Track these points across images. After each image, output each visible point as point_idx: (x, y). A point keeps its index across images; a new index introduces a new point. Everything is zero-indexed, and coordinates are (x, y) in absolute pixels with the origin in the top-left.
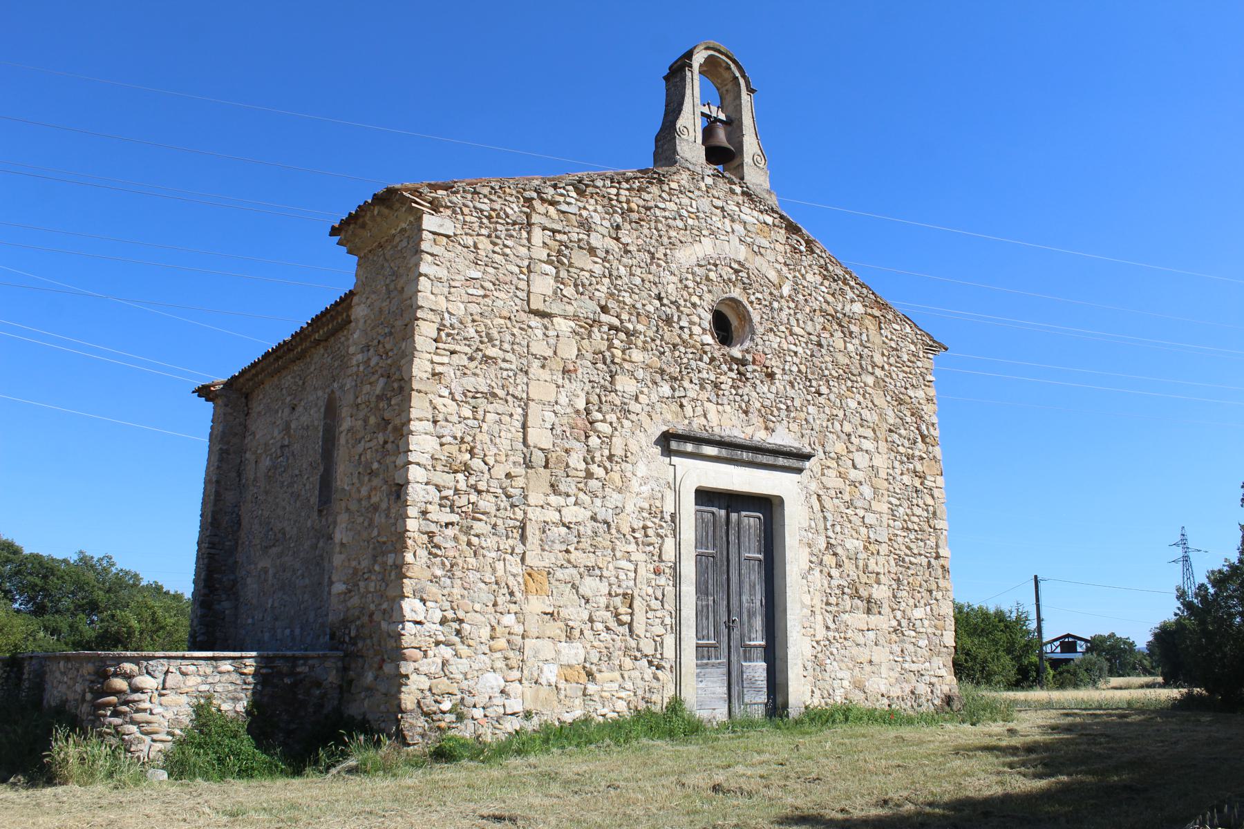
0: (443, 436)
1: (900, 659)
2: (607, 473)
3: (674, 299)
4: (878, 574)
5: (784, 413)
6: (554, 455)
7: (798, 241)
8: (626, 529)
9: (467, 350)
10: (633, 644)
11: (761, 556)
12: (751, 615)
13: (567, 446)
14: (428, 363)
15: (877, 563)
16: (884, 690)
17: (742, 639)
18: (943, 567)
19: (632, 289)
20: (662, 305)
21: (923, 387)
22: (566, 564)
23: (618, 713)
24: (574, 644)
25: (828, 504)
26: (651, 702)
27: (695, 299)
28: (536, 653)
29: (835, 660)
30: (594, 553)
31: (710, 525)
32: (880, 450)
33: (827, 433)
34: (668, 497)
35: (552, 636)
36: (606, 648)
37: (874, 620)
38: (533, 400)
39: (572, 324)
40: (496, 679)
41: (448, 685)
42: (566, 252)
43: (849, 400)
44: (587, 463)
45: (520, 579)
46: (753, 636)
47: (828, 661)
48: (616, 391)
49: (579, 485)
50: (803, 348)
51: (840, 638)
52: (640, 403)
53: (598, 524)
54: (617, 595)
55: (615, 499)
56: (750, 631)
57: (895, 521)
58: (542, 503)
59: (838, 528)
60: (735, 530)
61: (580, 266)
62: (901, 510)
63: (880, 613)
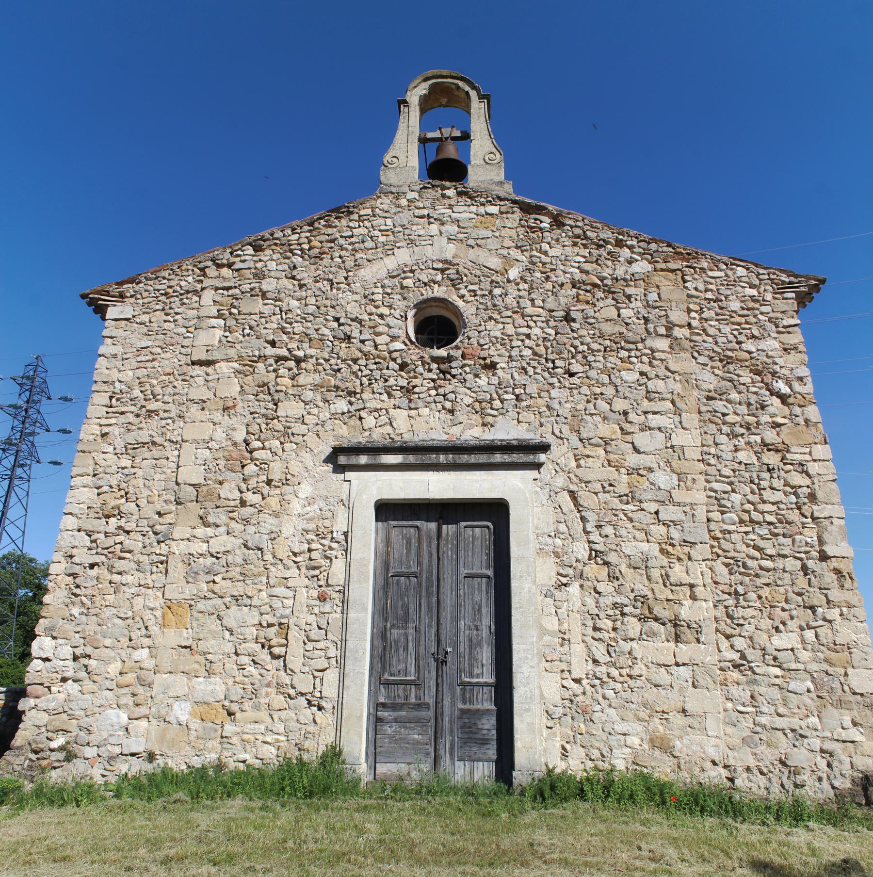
0: (101, 487)
1: (750, 709)
2: (263, 499)
3: (354, 317)
4: (692, 586)
5: (509, 405)
6: (205, 489)
7: (536, 219)
8: (283, 553)
9: (133, 409)
11: (490, 573)
12: (474, 644)
13: (220, 478)
14: (98, 427)
15: (687, 572)
16: (712, 753)
17: (459, 671)
18: (837, 572)
19: (305, 318)
20: (340, 325)
21: (776, 335)
23: (262, 759)
24: (212, 680)
25: (585, 498)
27: (385, 311)
28: (166, 688)
29: (610, 706)
30: (244, 581)
31: (414, 541)
32: (685, 425)
33: (584, 417)
34: (340, 515)
36: (252, 684)
37: (685, 651)
38: (187, 441)
39: (235, 365)
40: (118, 716)
41: (64, 722)
42: (236, 303)
43: (623, 373)
44: (241, 492)
45: (158, 613)
46: (476, 671)
47: (597, 708)
48: (278, 417)
49: (231, 515)
50: (542, 328)
51: (621, 675)
52: (306, 424)
53: (251, 551)
54: (270, 625)
55: (269, 523)
56: (471, 666)
57: (723, 513)
58: (188, 536)
59: (609, 530)
60: (452, 544)
61: (248, 312)
62: (736, 498)
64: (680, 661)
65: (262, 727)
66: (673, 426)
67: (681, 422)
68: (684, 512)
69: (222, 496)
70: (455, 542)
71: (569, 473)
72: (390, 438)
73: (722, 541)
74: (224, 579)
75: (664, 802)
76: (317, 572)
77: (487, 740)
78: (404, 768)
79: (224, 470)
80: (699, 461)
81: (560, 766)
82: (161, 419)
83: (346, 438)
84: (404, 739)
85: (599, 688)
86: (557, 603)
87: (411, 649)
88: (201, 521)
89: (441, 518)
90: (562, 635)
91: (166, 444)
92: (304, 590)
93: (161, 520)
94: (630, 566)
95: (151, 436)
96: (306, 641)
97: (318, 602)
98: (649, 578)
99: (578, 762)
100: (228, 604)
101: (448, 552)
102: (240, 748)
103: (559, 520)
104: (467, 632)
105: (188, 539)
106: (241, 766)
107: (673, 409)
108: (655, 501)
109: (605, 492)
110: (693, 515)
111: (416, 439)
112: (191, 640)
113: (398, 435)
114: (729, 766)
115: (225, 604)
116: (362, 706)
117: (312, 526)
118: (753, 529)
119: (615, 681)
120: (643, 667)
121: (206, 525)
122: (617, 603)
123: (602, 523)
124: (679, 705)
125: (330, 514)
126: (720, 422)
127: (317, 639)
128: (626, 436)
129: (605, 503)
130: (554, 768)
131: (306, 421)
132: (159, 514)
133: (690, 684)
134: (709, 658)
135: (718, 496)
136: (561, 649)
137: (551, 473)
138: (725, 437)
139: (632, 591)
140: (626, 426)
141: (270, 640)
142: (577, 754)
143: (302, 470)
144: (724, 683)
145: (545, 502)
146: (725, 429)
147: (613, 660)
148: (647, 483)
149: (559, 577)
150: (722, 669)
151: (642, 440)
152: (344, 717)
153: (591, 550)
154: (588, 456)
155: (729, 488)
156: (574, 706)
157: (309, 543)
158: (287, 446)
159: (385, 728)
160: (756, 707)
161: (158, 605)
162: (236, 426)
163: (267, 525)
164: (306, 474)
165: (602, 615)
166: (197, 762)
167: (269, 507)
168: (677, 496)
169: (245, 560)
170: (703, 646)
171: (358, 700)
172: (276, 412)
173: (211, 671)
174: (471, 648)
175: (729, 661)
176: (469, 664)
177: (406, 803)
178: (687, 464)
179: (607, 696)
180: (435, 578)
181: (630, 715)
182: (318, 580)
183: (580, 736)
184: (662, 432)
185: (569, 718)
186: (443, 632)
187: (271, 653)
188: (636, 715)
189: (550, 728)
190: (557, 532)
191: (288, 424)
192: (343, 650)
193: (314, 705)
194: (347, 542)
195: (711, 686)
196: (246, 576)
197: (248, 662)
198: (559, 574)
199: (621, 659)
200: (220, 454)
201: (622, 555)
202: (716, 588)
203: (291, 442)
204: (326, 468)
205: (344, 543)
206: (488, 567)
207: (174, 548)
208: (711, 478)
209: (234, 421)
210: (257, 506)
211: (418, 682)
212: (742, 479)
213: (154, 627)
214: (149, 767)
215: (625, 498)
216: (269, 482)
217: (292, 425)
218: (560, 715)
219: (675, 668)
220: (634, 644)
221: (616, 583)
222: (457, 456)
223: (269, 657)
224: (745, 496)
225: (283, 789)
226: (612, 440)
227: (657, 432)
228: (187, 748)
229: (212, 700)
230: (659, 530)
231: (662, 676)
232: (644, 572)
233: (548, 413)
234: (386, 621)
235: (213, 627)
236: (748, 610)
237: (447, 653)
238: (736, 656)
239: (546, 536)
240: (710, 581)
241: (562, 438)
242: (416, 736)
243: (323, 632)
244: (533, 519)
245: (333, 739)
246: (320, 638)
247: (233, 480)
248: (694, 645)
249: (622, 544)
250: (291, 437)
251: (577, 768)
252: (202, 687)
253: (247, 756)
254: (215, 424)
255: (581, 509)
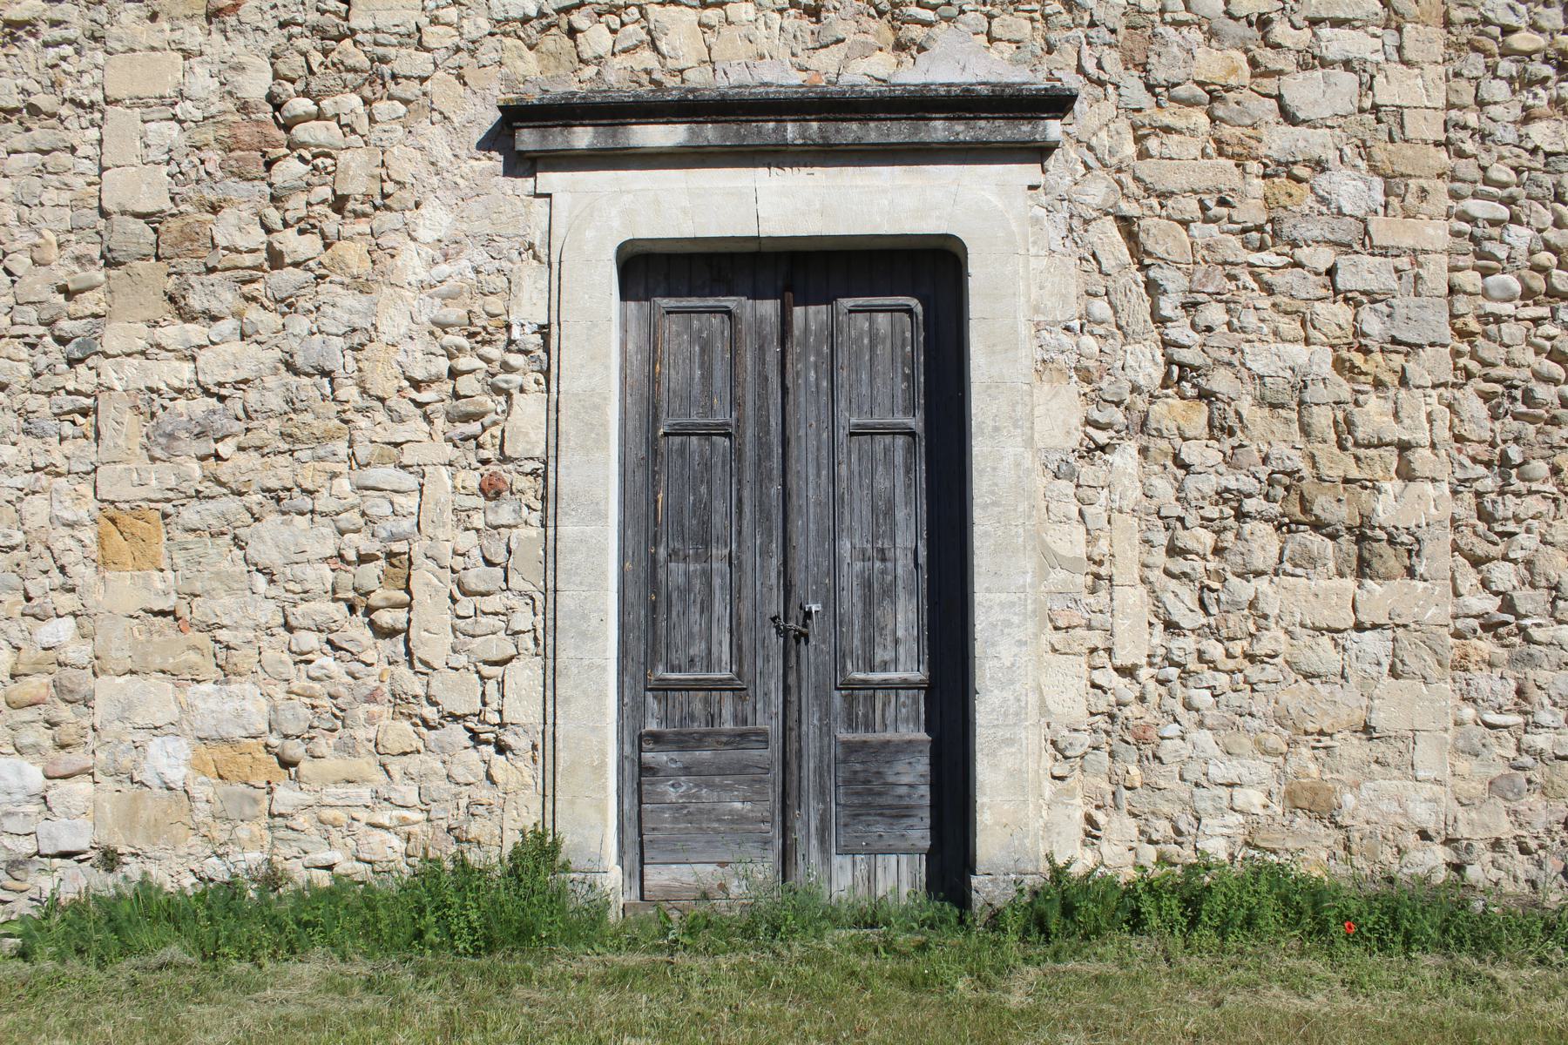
1: (1514, 719)
2: (327, 246)
4: (1404, 447)
6: (174, 224)
8: (385, 381)
10: (416, 686)
11: (916, 422)
12: (875, 593)
13: (213, 197)
15: (1396, 415)
16: (1424, 815)
17: (840, 656)
22: (210, 488)
23: (370, 862)
24: (233, 687)
25: (1160, 236)
26: (469, 841)
28: (125, 711)
29: (1201, 724)
30: (292, 452)
32: (1409, 54)
33: (1160, 29)
34: (527, 283)
35: (167, 667)
36: (332, 697)
37: (1379, 597)
38: (117, 102)
40: (19, 772)
44: (269, 231)
45: (88, 535)
46: (881, 655)
47: (1172, 730)
48: (353, 32)
49: (246, 289)
51: (1229, 655)
52: (428, 50)
53: (305, 380)
54: (363, 559)
55: (345, 306)
56: (869, 643)
57: (1486, 273)
58: (141, 345)
59: (1214, 314)
60: (818, 353)
62: (1520, 236)
63: (1411, 572)
64: (1366, 619)
65: (365, 794)
66: (1380, 57)
67: (1400, 49)
68: (1397, 270)
69: (221, 241)
70: (826, 349)
71: (1119, 170)
72: (652, 81)
73: (1480, 340)
74: (241, 449)
75: (1322, 929)
76: (474, 427)
77: (912, 807)
78: (707, 873)
79: (219, 174)
80: (1437, 144)
81: (1082, 861)
82: (46, 45)
83: (534, 83)
84: (710, 812)
85: (1176, 685)
86: (1083, 492)
87: (720, 608)
88: (171, 307)
89: (788, 288)
90: (1094, 568)
91: (65, 111)
92: (444, 472)
93: (71, 307)
94: (1261, 401)
95: (23, 91)
96: (457, 595)
97: (480, 502)
98: (1305, 430)
99: (1123, 848)
100: (256, 509)
101: (808, 374)
102: (317, 838)
103: (1093, 289)
104: (858, 566)
105: (143, 353)
106: (323, 879)
107: (1383, 13)
108: (1328, 242)
109: (1207, 220)
110: (1417, 277)
111: (722, 83)
112: (174, 597)
113: (672, 73)
114: (1457, 840)
115: (249, 510)
116: (603, 742)
117: (455, 313)
118: (1554, 311)
119: (1216, 669)
120: (1283, 637)
121: (187, 316)
122: (1227, 490)
123: (1200, 297)
124: (1358, 717)
125: (501, 282)
126: (1496, 50)
127: (482, 588)
128: (1265, 81)
129: (1208, 247)
130: (1068, 865)
131: (428, 40)
132: (68, 293)
133: (1386, 668)
134: (1432, 611)
135: (1478, 232)
136: (1091, 600)
137: (1073, 172)
138: (1504, 85)
139: (1265, 460)
140: (1266, 56)
141: (367, 594)
142: (1119, 830)
143: (423, 170)
144: (1461, 665)
145: (1056, 244)
146: (1507, 67)
147: (1212, 621)
148: (1310, 200)
149: (1090, 430)
150: (1458, 635)
151: (1303, 90)
152: (559, 769)
153: (1170, 362)
154: (1168, 130)
155: (1503, 212)
156: (1117, 728)
157: (450, 357)
158: (382, 108)
159: (661, 788)
160: (1526, 713)
161: (83, 514)
162: (243, 59)
163: (338, 313)
164: (435, 180)
165: (1192, 519)
166: (217, 869)
167: (343, 266)
168: (1382, 231)
169: (290, 402)
170: (1420, 585)
171: (594, 729)
172: (346, 19)
173: (229, 668)
174: (868, 601)
175: (1475, 617)
176: (863, 640)
177: (721, 959)
178: (1410, 153)
179: (1196, 703)
180: (775, 439)
181: (1247, 743)
182: (479, 446)
183: (1127, 794)
184: (1353, 70)
185: (1103, 755)
186: (797, 565)
187: (372, 624)
188: (1258, 742)
189: (1061, 778)
190: (1088, 319)
191: (380, 51)
192: (550, 615)
193: (487, 742)
194: (546, 348)
195: (1434, 671)
196: (296, 440)
197: (317, 646)
198: (1089, 422)
199: (1233, 619)
200: (208, 134)
201: (1244, 374)
202: (1460, 451)
203: (390, 98)
204: (485, 163)
205: (540, 353)
206: (910, 409)
207: (110, 376)
208: (1465, 188)
209: (237, 47)
210: (312, 264)
211: (738, 684)
212: (1537, 191)
213: (81, 568)
214: (105, 883)
215: (1255, 235)
216: (339, 204)
217: (391, 52)
218: (1085, 748)
219: (1354, 635)
220: (1263, 584)
221: (1228, 443)
222: (831, 126)
223: (369, 633)
224: (1540, 231)
225: (419, 935)
226: (1228, 89)
227: (1339, 73)
228: (192, 840)
229: (238, 733)
230: (1334, 315)
231: (1324, 654)
232: (1295, 416)
233: (1066, 18)
234: (656, 544)
235: (225, 565)
236: (1529, 500)
237: (808, 615)
238: (1491, 605)
239: (1058, 329)
240: (1447, 434)
241: (1101, 83)
242: (738, 805)
243: (499, 571)
244: (1028, 287)
245: (537, 818)
246: (492, 587)
247: (246, 197)
248: (1401, 583)
249: (1246, 347)
250: (391, 85)
251: (1119, 862)
252: (212, 704)
253: (335, 856)
254: (187, 55)
255: (1147, 261)
